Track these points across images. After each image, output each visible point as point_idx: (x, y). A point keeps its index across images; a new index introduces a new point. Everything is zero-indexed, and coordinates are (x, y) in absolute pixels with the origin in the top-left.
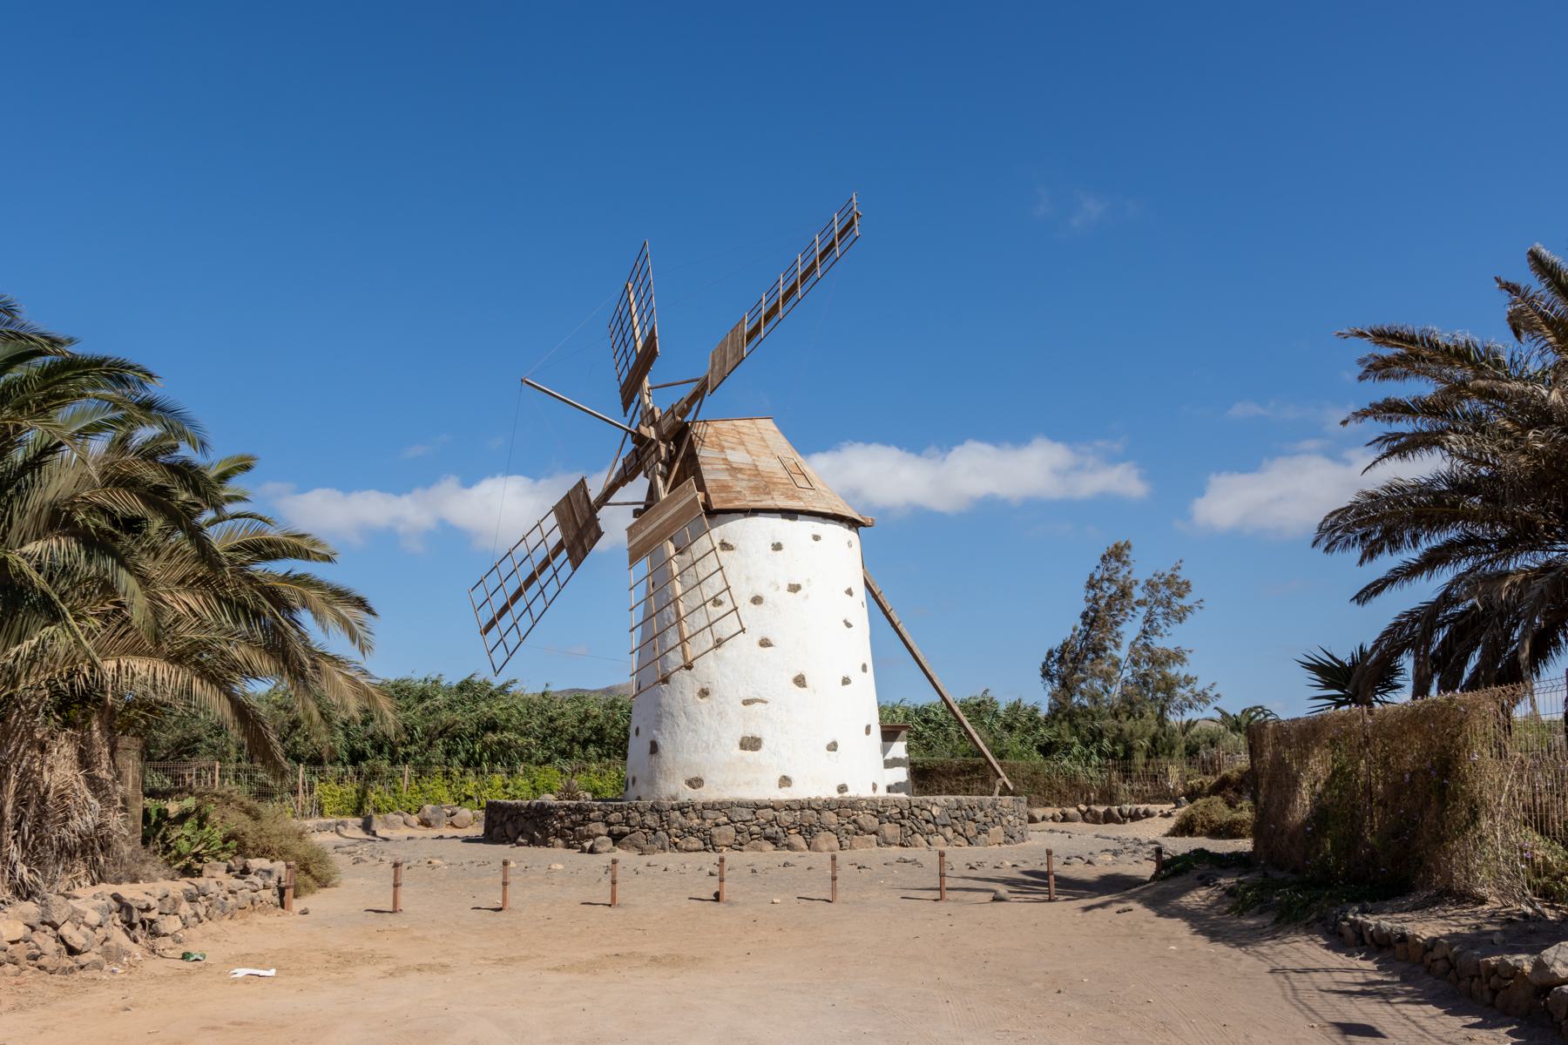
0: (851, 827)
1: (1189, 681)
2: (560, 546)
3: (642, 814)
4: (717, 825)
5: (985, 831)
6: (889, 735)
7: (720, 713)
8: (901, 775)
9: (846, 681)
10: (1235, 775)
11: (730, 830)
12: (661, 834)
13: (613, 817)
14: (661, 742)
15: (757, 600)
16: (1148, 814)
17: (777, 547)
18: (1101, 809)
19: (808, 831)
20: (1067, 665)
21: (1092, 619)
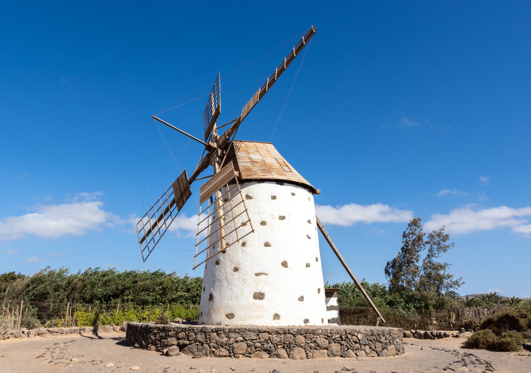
0: (313, 345)
1: (449, 277)
2: (174, 202)
3: (196, 334)
4: (237, 342)
5: (386, 348)
6: (329, 293)
7: (243, 280)
8: (335, 314)
9: (308, 265)
10: (496, 318)
11: (244, 345)
12: (206, 345)
13: (181, 335)
14: (214, 294)
15: (263, 223)
16: (446, 336)
17: (274, 198)
18: (422, 332)
19: (288, 347)
20: (395, 269)
21: (405, 250)
